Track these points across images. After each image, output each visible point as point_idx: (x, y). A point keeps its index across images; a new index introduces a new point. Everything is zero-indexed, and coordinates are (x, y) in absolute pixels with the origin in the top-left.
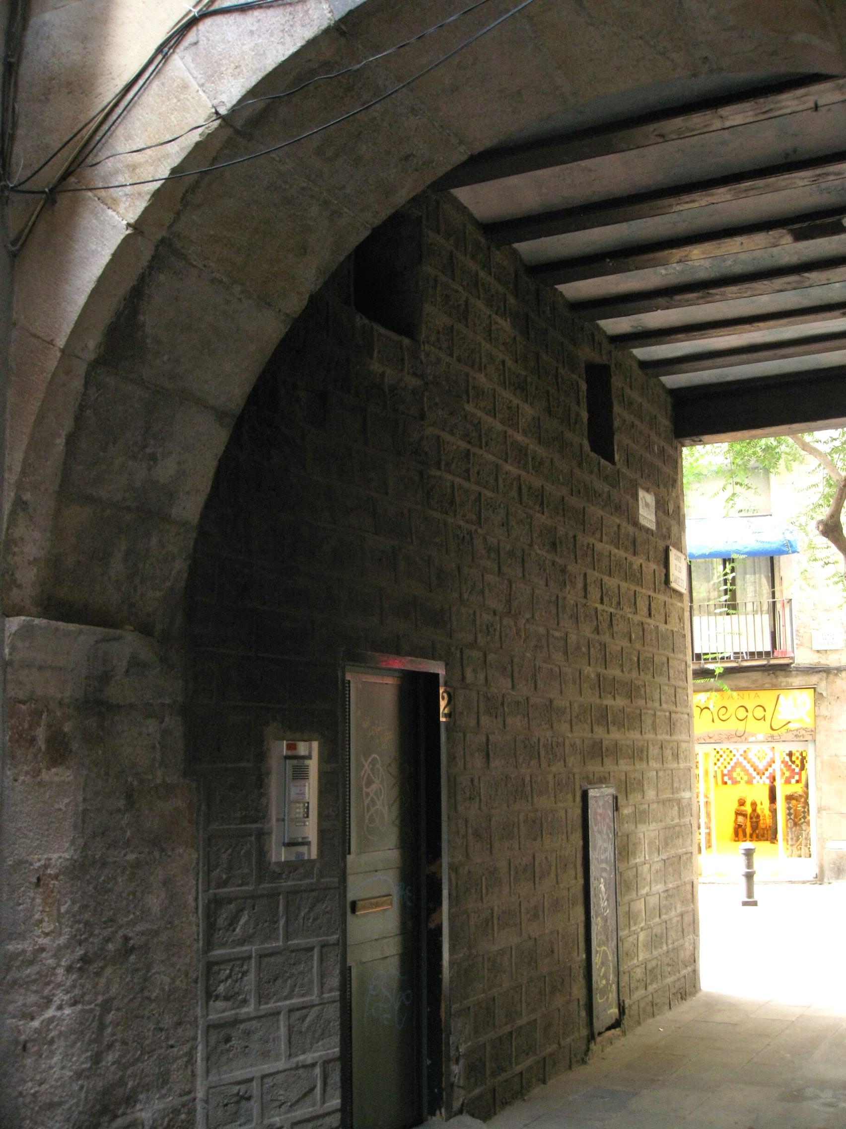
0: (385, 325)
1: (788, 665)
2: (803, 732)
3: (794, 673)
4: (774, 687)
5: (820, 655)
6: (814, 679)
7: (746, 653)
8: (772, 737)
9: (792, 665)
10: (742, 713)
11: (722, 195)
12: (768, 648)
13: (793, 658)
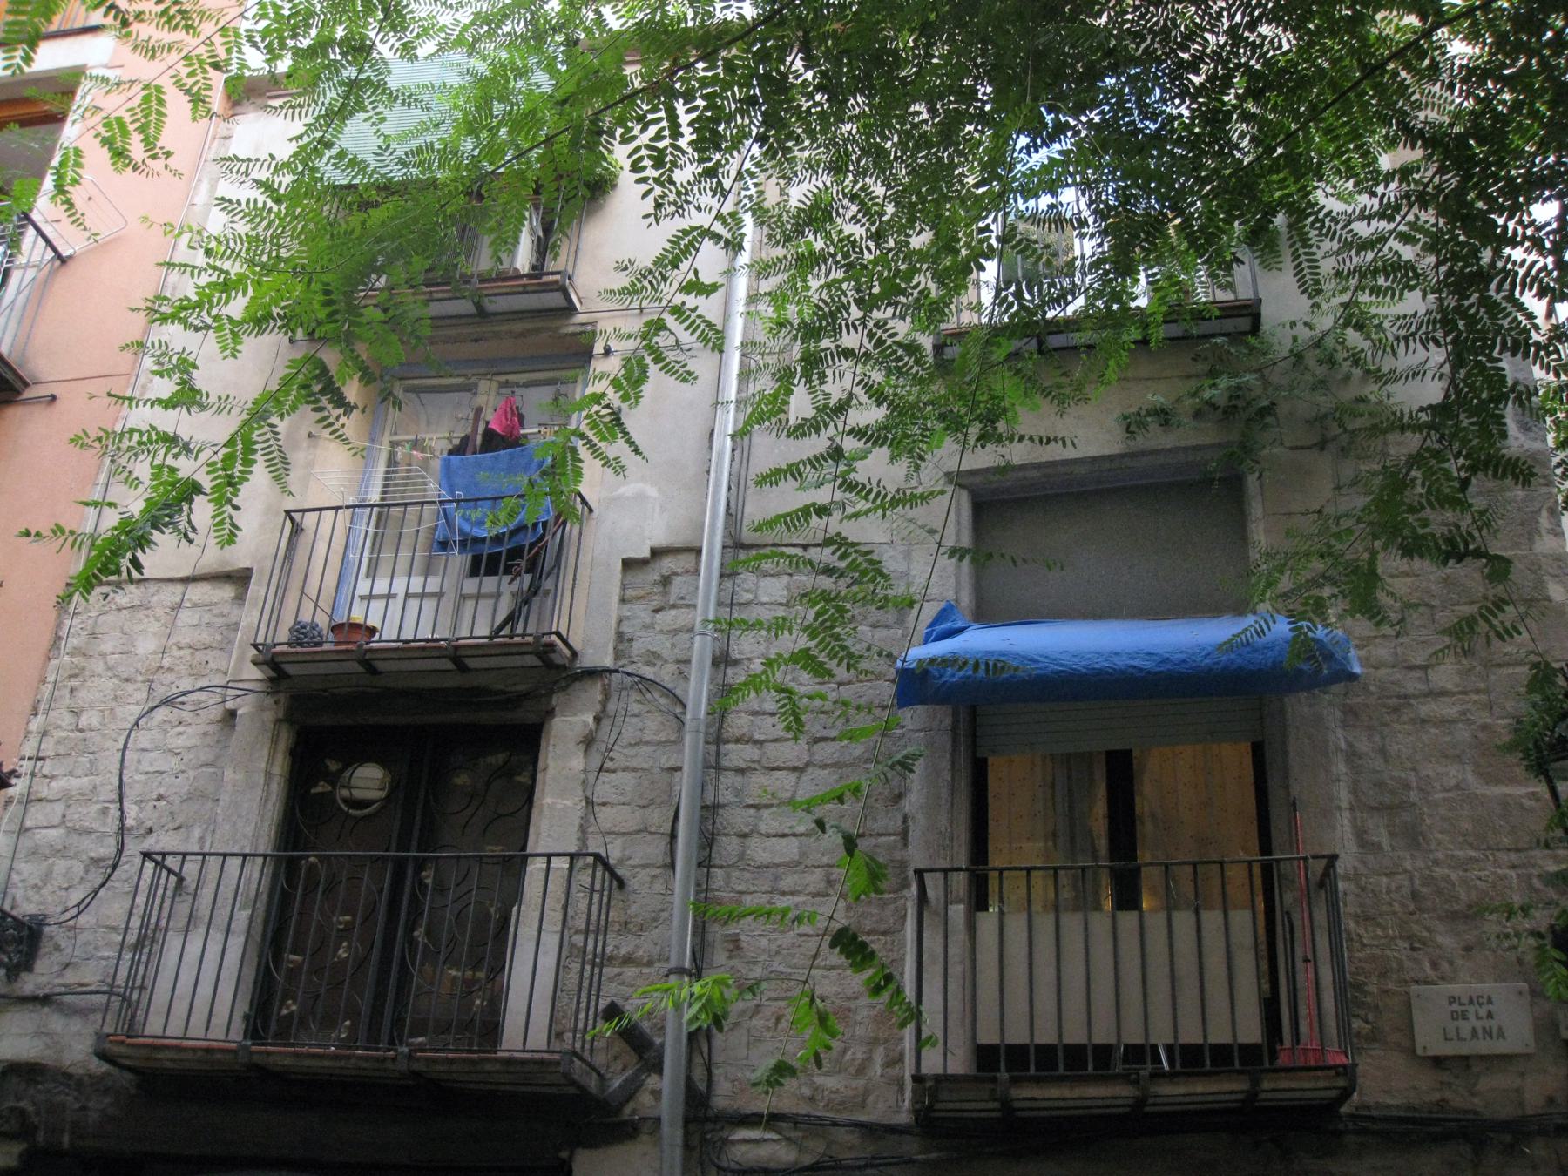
1: (1329, 1108)
7: (1169, 1049)
9: (1344, 1109)
11: (1051, 972)
12: (1251, 1031)
13: (1348, 1072)
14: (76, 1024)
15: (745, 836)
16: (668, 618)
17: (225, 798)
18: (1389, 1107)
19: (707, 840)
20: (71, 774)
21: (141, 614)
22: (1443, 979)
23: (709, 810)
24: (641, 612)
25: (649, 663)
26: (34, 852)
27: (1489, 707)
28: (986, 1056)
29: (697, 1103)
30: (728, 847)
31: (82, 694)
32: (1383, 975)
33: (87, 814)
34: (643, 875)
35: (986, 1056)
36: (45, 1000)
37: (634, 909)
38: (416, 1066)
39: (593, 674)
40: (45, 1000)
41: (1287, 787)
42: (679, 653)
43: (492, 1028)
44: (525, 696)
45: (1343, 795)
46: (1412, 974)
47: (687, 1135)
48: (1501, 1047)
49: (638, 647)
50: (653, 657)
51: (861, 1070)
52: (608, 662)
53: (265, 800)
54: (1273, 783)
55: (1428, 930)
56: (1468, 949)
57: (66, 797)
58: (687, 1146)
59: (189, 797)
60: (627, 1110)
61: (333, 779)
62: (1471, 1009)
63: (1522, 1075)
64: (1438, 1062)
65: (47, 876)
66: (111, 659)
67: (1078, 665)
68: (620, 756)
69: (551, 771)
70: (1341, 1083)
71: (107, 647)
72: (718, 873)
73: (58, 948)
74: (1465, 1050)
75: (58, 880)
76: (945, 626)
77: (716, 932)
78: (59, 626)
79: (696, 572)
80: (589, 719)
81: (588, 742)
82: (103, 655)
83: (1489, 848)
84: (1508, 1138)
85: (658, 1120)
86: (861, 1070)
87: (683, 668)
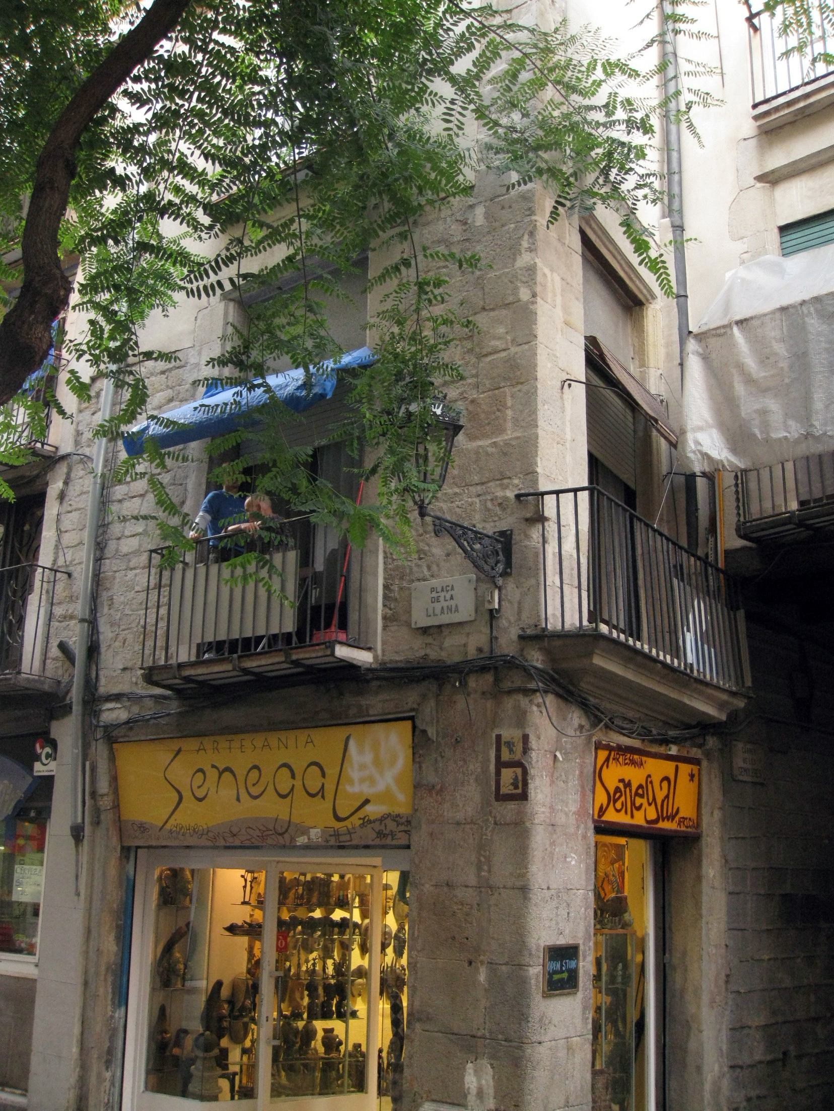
0: (34, 197)
2: (391, 825)
3: (375, 684)
4: (338, 720)
5: (429, 640)
6: (410, 697)
8: (337, 834)
10: (284, 782)
18: (397, 662)
22: (432, 576)
27: (477, 386)
30: (112, 546)
32: (402, 578)
39: (64, 458)
46: (416, 575)
55: (428, 545)
56: (448, 555)
62: (442, 594)
63: (468, 635)
64: (425, 631)
74: (436, 622)
83: (467, 485)
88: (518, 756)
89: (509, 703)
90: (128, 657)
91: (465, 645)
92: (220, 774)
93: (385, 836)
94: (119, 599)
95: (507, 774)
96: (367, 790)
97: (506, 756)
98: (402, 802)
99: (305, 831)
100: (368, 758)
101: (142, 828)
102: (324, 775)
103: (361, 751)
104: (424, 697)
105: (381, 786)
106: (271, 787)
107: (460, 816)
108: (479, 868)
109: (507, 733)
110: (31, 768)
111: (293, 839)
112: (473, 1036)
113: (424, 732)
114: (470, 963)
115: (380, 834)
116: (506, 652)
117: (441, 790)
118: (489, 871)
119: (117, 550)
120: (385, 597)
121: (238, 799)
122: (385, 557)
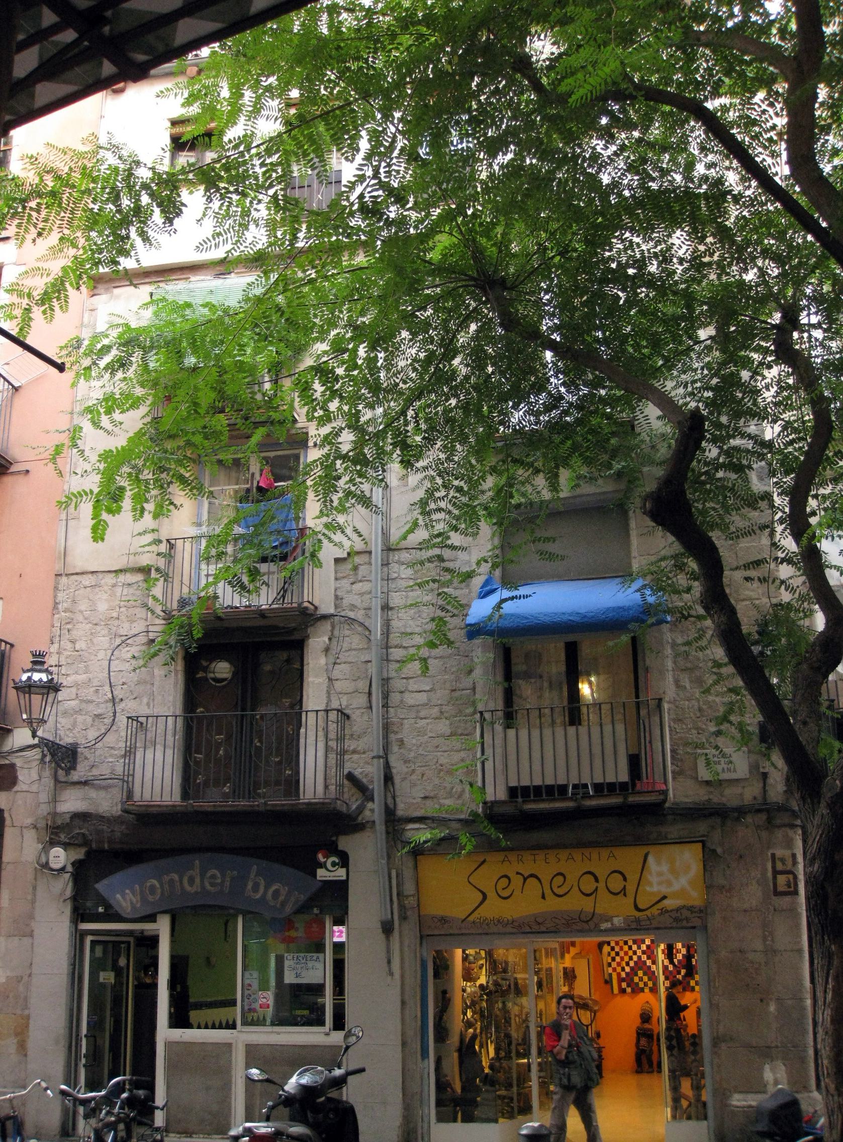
4: (639, 841)
5: (712, 789)
6: (702, 827)
8: (638, 921)
9: (667, 805)
10: (588, 885)
14: (102, 793)
15: (402, 692)
16: (358, 587)
17: (157, 683)
19: (386, 696)
20: (76, 673)
21: (97, 589)
23: (386, 681)
24: (345, 583)
25: (351, 610)
26: (65, 713)
28: (513, 792)
29: (390, 814)
30: (395, 698)
31: (74, 632)
33: (88, 693)
34: (358, 712)
35: (513, 792)
36: (85, 783)
37: (355, 728)
38: (269, 808)
39: (325, 617)
40: (85, 783)
41: (644, 661)
42: (365, 605)
43: (293, 785)
44: (295, 629)
45: (669, 664)
47: (387, 827)
48: (734, 776)
49: (345, 602)
50: (353, 607)
51: (460, 797)
52: (332, 611)
53: (176, 684)
54: (640, 658)
57: (77, 685)
58: (388, 833)
59: (139, 683)
60: (360, 818)
61: (205, 669)
64: (708, 783)
65: (74, 725)
66: (87, 614)
67: (547, 619)
68: (342, 658)
69: (311, 666)
70: (662, 797)
71: (83, 608)
72: (391, 710)
73: (86, 758)
75: (80, 726)
76: (488, 588)
77: (392, 737)
78: (55, 597)
79: (370, 564)
80: (326, 639)
81: (327, 650)
82: (81, 612)
84: (736, 814)
85: (374, 822)
86: (460, 797)
87: (368, 612)
88: (789, 867)
89: (779, 834)
90: (429, 788)
91: (741, 795)
92: (525, 879)
93: (681, 920)
94: (411, 740)
95: (782, 879)
96: (664, 890)
97: (779, 866)
98: (696, 897)
99: (609, 919)
100: (665, 868)
101: (443, 920)
102: (625, 879)
103: (659, 863)
104: (713, 827)
105: (676, 887)
106: (576, 888)
107: (746, 906)
108: (765, 939)
109: (779, 853)
110: (315, 876)
111: (597, 925)
112: (769, 1047)
113: (714, 851)
114: (762, 1000)
115: (676, 920)
116: (775, 800)
117: (729, 890)
118: (773, 941)
119: (402, 701)
120: (672, 757)
121: (543, 897)
122: (670, 730)
